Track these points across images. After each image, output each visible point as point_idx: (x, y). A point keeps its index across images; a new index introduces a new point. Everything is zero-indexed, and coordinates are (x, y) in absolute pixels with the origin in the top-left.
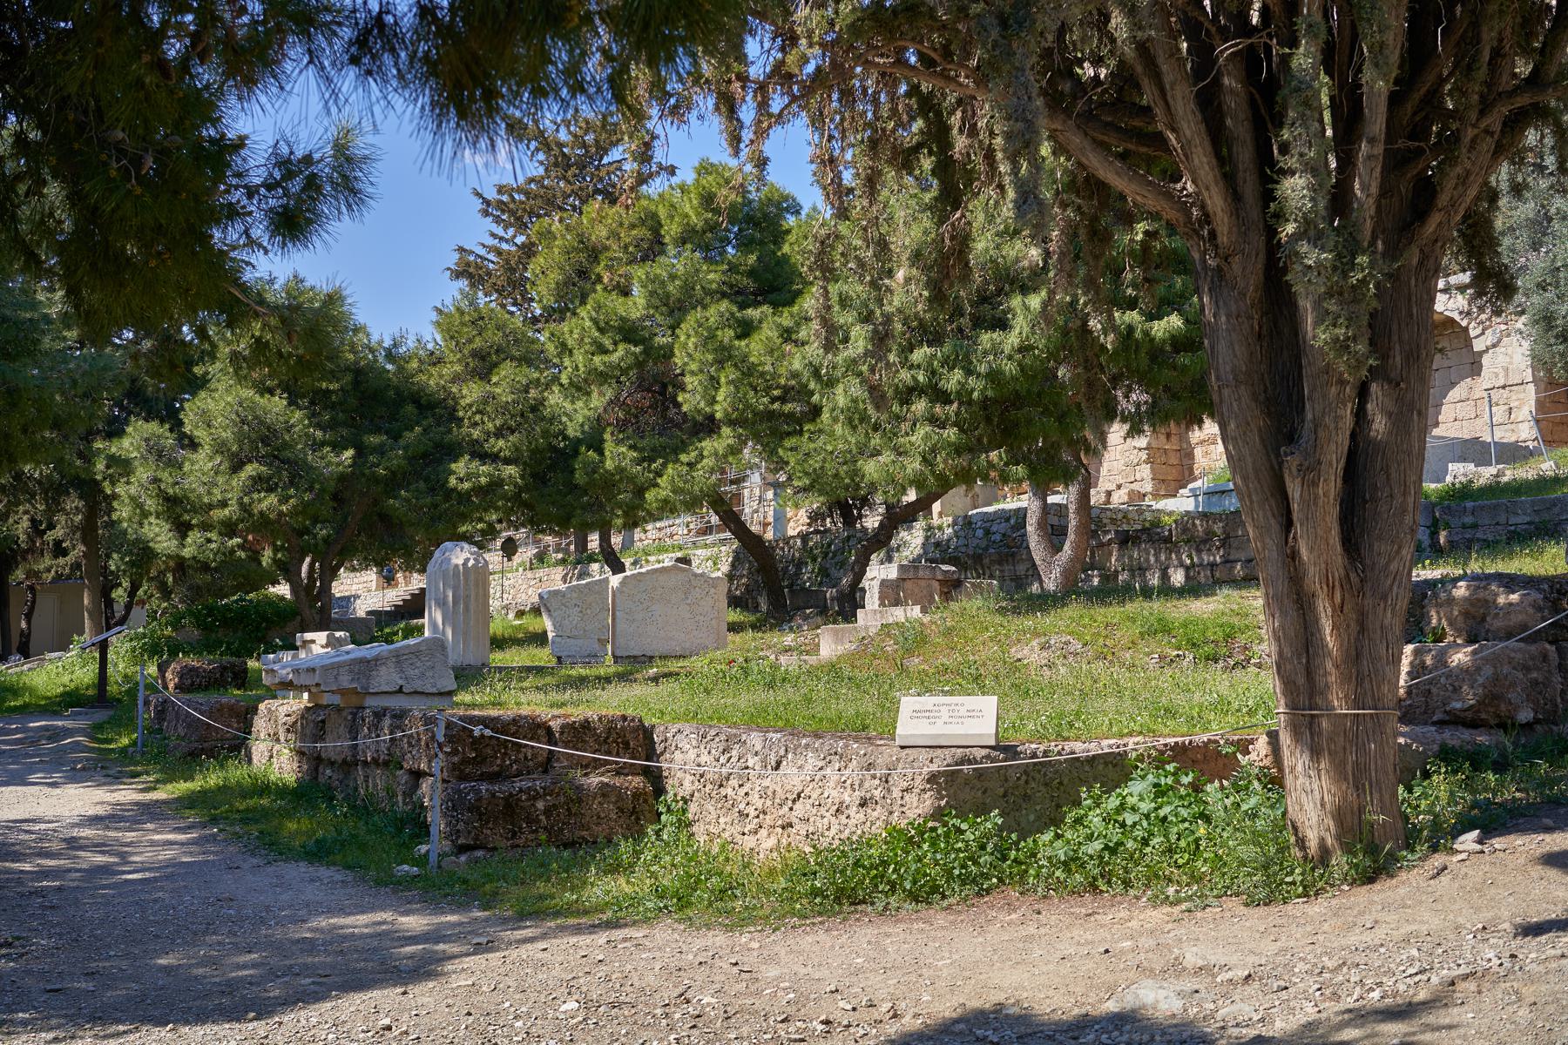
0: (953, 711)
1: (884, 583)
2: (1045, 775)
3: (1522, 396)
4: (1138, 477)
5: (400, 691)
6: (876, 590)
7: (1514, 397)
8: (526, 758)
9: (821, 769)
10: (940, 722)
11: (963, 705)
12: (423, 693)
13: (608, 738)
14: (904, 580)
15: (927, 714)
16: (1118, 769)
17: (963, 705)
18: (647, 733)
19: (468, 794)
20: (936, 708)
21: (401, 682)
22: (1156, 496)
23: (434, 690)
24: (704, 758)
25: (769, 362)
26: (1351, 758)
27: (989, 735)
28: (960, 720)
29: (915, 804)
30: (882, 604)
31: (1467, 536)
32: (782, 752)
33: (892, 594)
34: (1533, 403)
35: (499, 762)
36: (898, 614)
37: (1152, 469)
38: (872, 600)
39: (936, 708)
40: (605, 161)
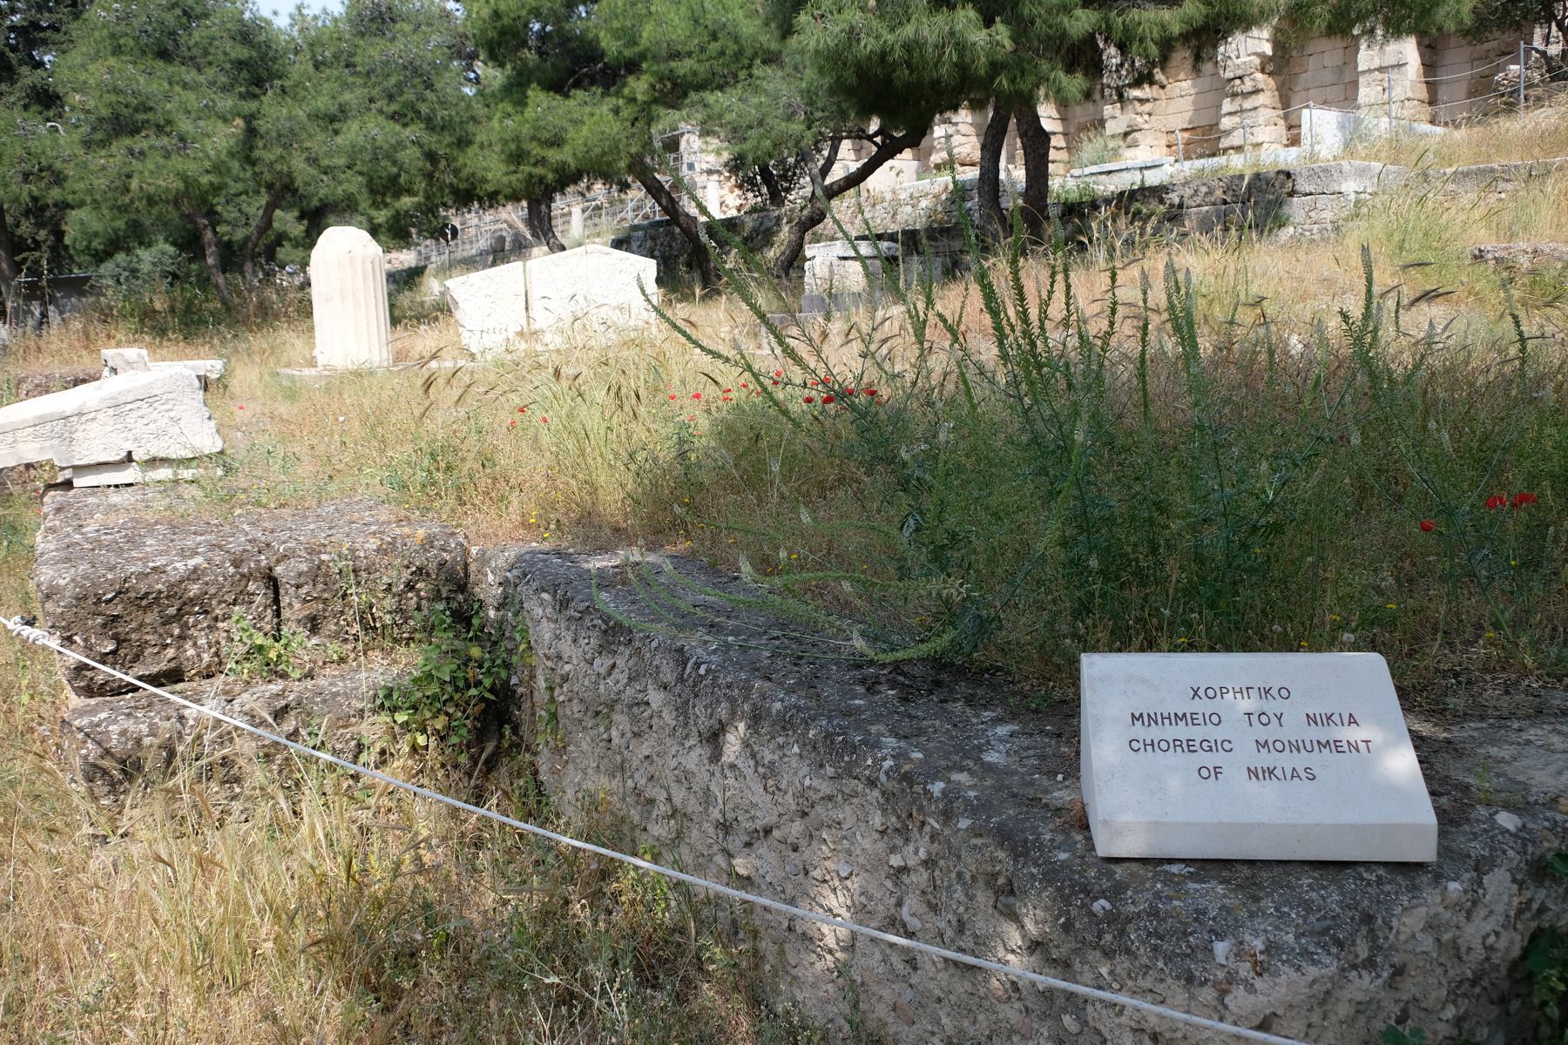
5: (129, 458)
10: (1234, 766)
11: (1285, 693)
15: (1182, 731)
17: (1285, 693)
20: (1201, 706)
24: (566, 647)
28: (1300, 760)
35: (171, 652)
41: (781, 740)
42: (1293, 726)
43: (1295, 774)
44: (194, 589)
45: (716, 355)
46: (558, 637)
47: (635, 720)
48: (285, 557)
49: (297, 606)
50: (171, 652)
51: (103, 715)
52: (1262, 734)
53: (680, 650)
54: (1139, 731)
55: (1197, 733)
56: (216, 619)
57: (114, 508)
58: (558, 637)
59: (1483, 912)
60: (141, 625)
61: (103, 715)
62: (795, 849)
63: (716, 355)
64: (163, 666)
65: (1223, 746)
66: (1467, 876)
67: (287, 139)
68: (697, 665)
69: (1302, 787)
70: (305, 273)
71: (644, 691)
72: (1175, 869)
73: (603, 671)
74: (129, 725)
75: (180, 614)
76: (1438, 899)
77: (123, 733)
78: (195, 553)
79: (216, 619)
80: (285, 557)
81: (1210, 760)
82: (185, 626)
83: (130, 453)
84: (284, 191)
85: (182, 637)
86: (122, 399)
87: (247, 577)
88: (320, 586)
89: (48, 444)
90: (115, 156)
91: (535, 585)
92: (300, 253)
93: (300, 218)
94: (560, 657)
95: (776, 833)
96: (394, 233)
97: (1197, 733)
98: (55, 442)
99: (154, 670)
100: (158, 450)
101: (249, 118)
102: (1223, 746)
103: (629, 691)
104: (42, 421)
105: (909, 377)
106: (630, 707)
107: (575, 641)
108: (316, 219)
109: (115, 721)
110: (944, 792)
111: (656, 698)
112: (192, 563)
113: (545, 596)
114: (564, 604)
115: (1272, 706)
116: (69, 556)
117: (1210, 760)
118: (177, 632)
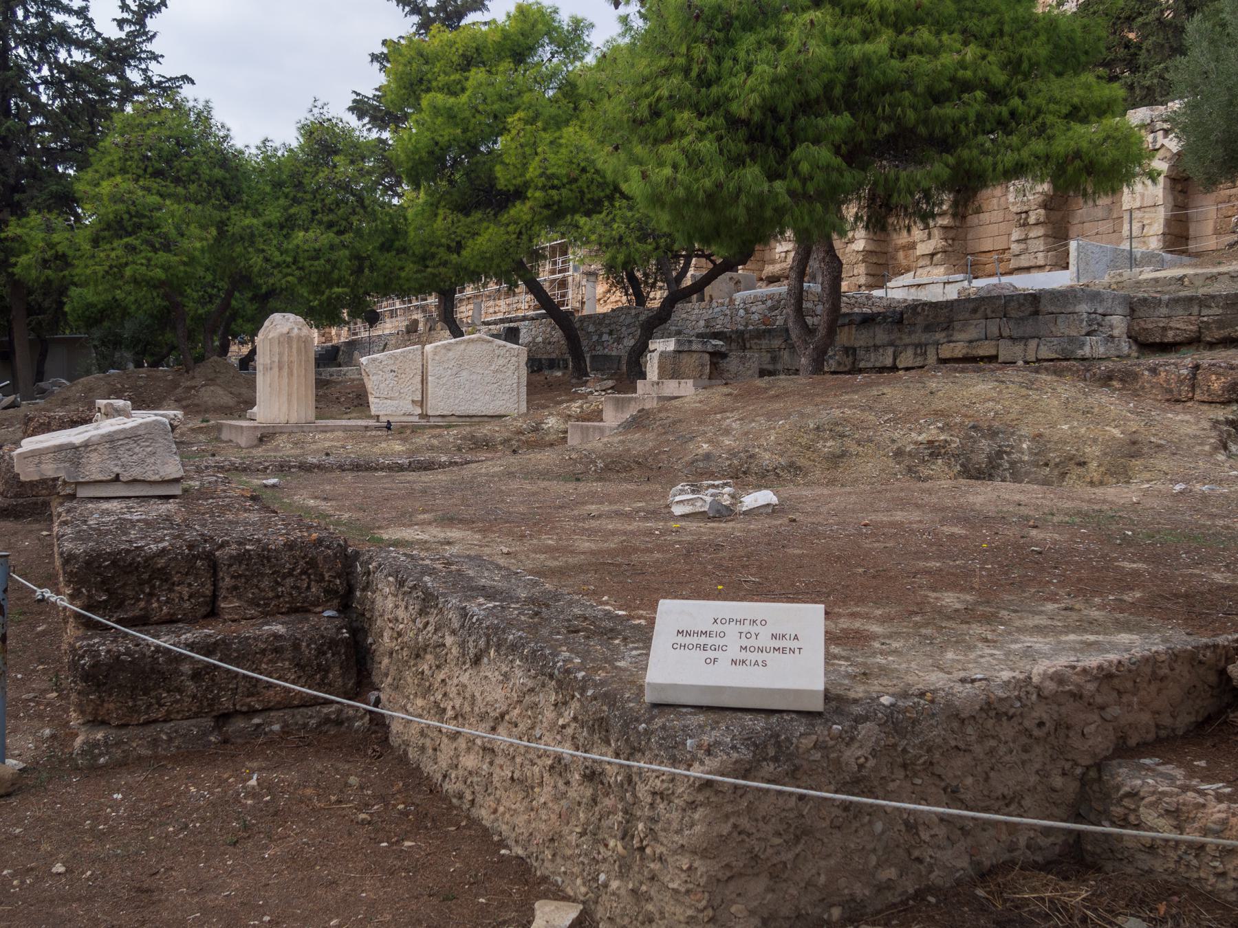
0: (748, 635)
1: (662, 354)
2: (904, 751)
3: (1153, 215)
4: (856, 272)
5: (117, 479)
6: (656, 361)
7: (1147, 216)
8: (181, 598)
9: (532, 690)
10: (724, 658)
11: (764, 623)
12: (144, 481)
13: (293, 569)
14: (680, 352)
15: (703, 640)
16: (1015, 721)
17: (764, 623)
18: (346, 561)
19: (82, 657)
20: (718, 628)
21: (117, 470)
22: (871, 287)
23: (157, 478)
24: (401, 613)
25: (1063, 762)
26: (1077, 520)
27: (812, 693)
28: (760, 657)
29: (675, 826)
30: (661, 376)
31: (1161, 325)
32: (482, 643)
33: (671, 369)
34: (1162, 221)
35: (142, 604)
36: (671, 387)
37: (867, 267)
38: (652, 371)
39: (718, 628)
40: (463, 23)
41: (510, 658)
42: (765, 640)
43: (756, 663)
44: (161, 562)
45: (1052, 360)
46: (397, 607)
47: (437, 657)
48: (222, 546)
49: (227, 579)
50: (142, 604)
51: (96, 640)
52: (745, 642)
53: (464, 608)
54: (681, 640)
55: (710, 641)
56: (173, 584)
57: (108, 513)
58: (397, 607)
59: (857, 745)
60: (125, 584)
61: (96, 640)
62: (516, 726)
63: (1052, 360)
64: (137, 613)
65: (722, 648)
66: (847, 724)
67: (250, 237)
68: (472, 616)
69: (760, 670)
70: (253, 342)
71: (443, 637)
72: (684, 710)
73: (421, 626)
74: (114, 647)
75: (151, 579)
76: (826, 733)
77: (108, 651)
78: (162, 540)
79: (173, 584)
80: (222, 546)
81: (712, 654)
82: (153, 587)
83: (118, 475)
84: (242, 280)
85: (151, 595)
86: (117, 437)
87: (196, 557)
88: (244, 567)
89: (62, 465)
90: (115, 250)
91: (385, 572)
92: (248, 327)
93: (252, 300)
94: (397, 620)
95: (507, 717)
96: (323, 315)
97: (710, 641)
98: (67, 465)
99: (130, 614)
100: (136, 473)
101: (221, 225)
102: (722, 648)
103: (435, 637)
104: (60, 448)
105: (1013, 416)
106: (435, 647)
107: (406, 608)
108: (267, 303)
109: (104, 644)
110: (583, 677)
111: (449, 640)
112: (161, 545)
113: (391, 579)
114: (401, 583)
115: (754, 629)
116: (79, 537)
117: (712, 654)
118: (147, 590)
